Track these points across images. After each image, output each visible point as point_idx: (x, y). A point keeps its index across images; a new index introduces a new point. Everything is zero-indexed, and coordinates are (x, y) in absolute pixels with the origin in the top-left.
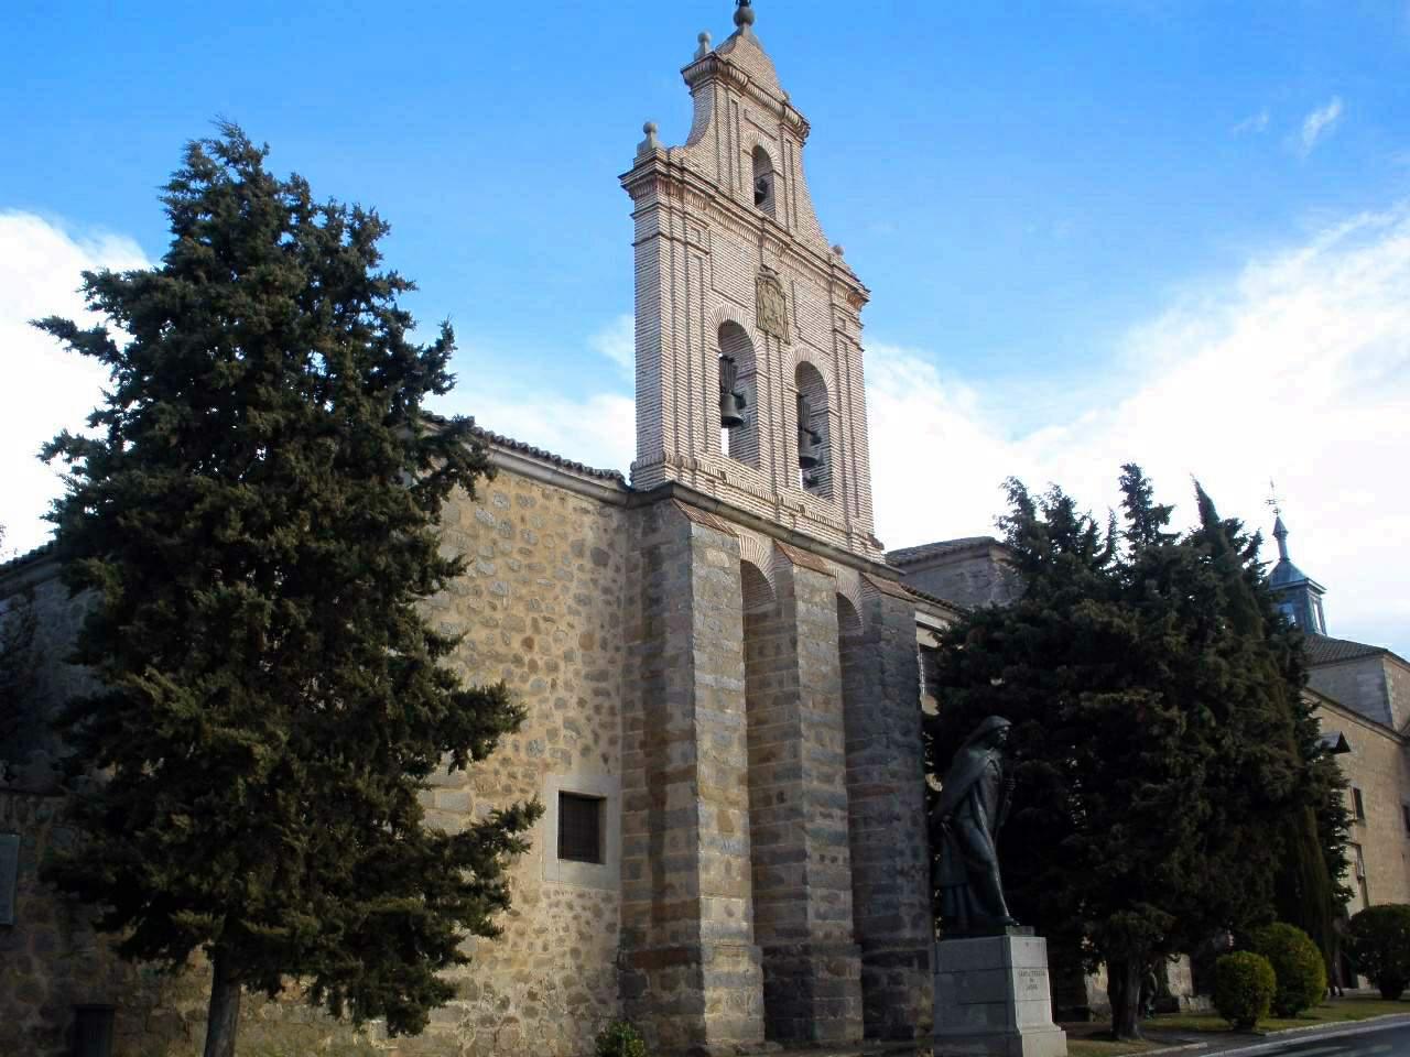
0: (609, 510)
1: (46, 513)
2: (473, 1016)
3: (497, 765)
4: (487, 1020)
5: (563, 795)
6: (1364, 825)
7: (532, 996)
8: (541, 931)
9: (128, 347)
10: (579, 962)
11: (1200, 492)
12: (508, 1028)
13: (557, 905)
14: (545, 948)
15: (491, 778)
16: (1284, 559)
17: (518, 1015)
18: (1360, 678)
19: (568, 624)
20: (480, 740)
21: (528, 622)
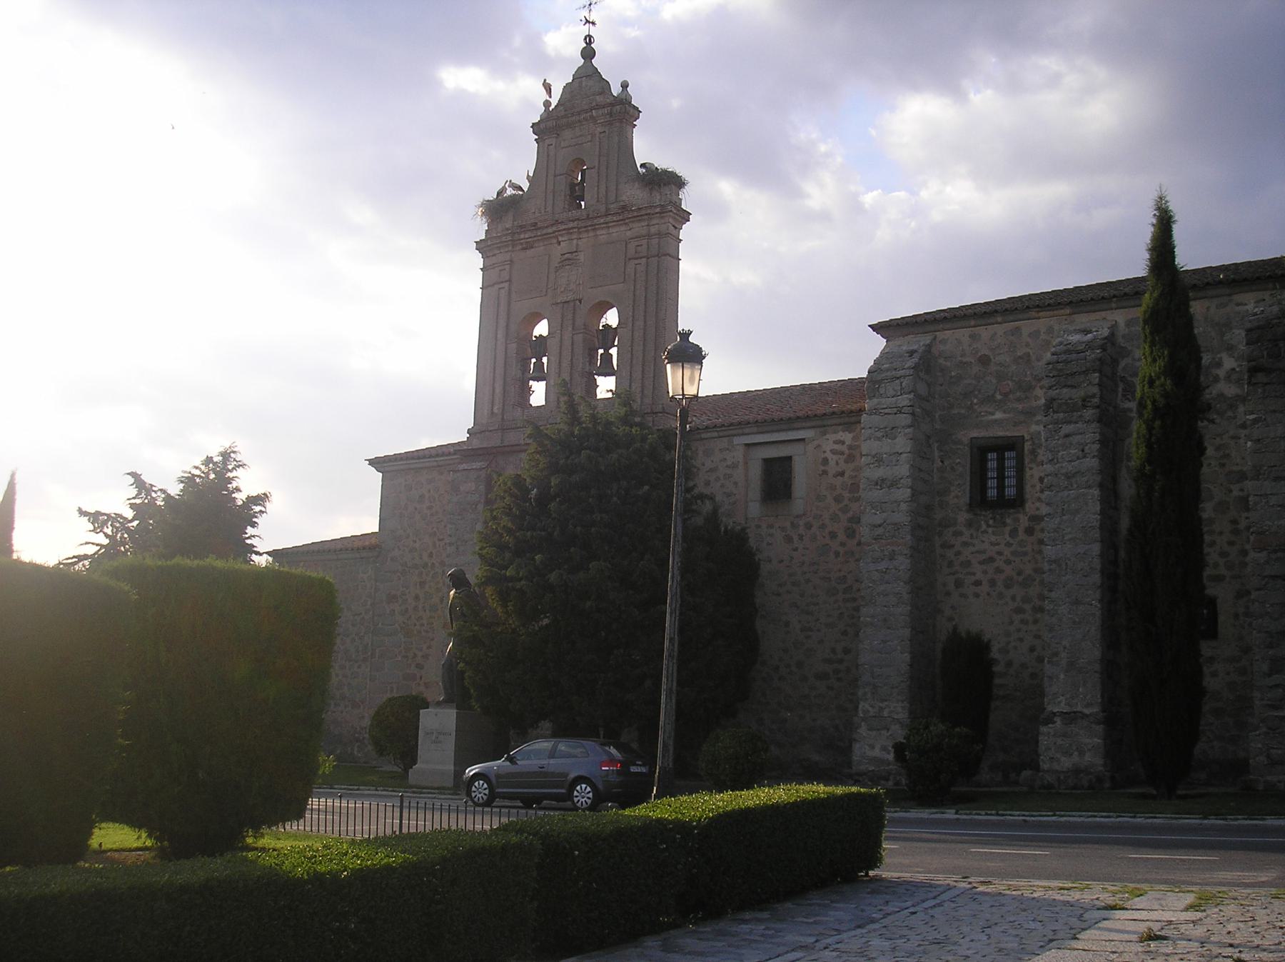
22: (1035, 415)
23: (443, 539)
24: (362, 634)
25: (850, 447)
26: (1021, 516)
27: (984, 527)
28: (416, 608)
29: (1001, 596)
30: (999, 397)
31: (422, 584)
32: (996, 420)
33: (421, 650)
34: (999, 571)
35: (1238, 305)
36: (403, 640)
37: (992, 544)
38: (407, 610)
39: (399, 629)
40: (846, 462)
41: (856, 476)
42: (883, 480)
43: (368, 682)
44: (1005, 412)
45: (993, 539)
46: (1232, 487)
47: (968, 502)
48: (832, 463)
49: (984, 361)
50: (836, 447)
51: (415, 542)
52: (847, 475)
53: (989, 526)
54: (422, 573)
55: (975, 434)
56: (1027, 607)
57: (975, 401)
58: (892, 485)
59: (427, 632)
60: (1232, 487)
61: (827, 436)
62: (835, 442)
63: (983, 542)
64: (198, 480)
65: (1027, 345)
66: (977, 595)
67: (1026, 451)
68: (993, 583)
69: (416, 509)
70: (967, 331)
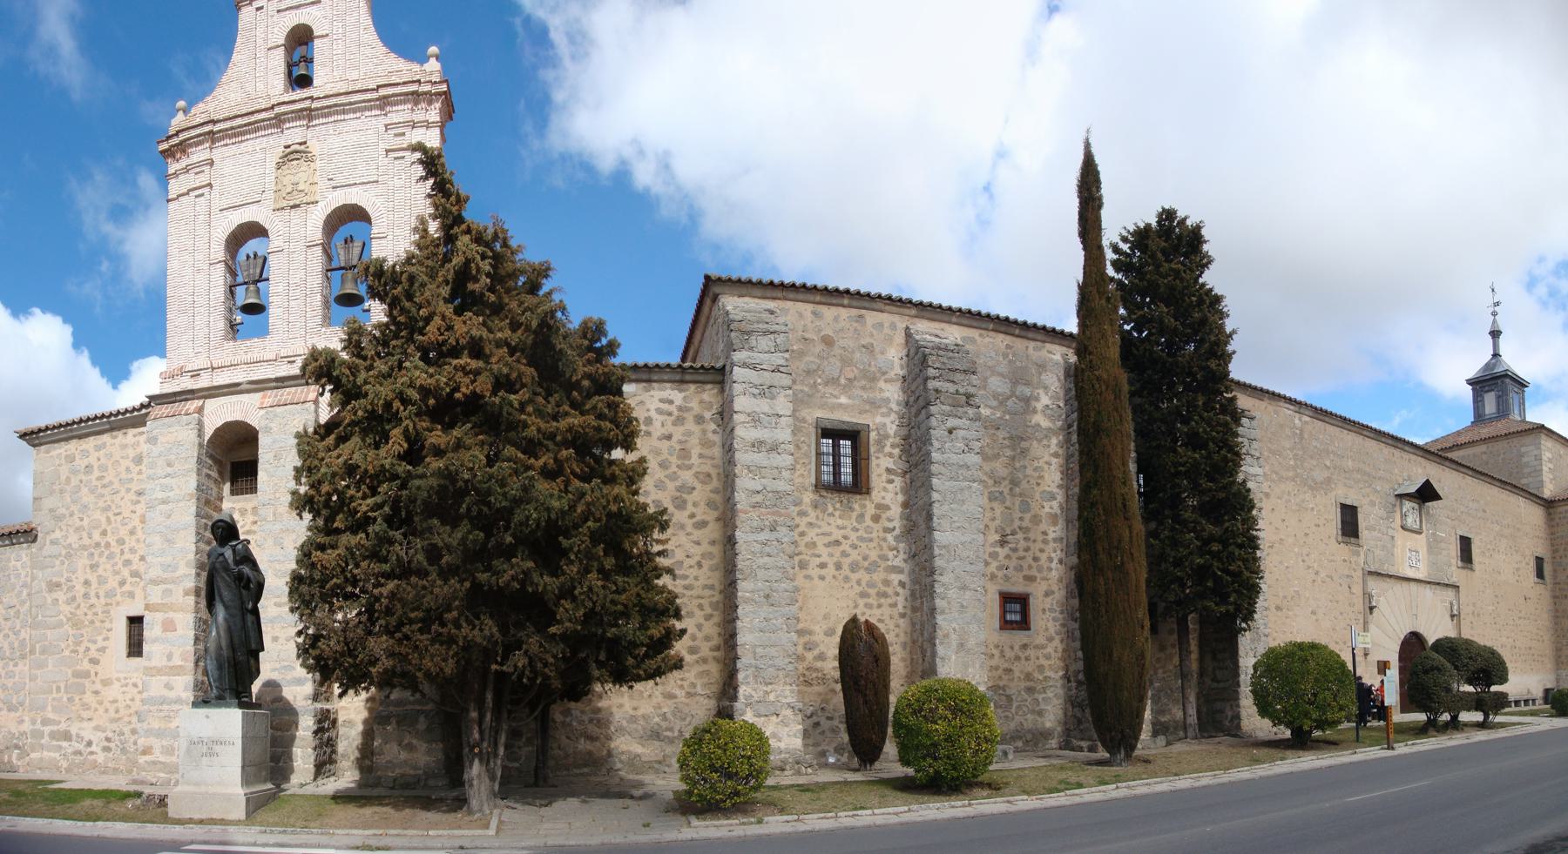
2: (70, 750)
3: (86, 610)
4: (79, 753)
6: (1472, 569)
7: (108, 740)
8: (115, 701)
9: (22, 318)
11: (1087, 146)
12: (91, 757)
13: (126, 685)
14: (117, 711)
15: (82, 617)
16: (1496, 355)
18: (1523, 449)
20: (555, 141)
21: (103, 520)
22: (880, 407)
23: (119, 514)
24: (18, 628)
25: (680, 409)
26: (867, 502)
27: (831, 509)
28: (86, 595)
29: (847, 579)
30: (843, 381)
31: (94, 567)
32: (841, 404)
33: (95, 642)
34: (844, 554)
35: (1050, 352)
36: (71, 632)
37: (838, 527)
38: (74, 598)
39: (65, 620)
40: (674, 424)
41: (686, 441)
42: (761, 442)
43: (27, 681)
44: (850, 398)
45: (840, 522)
46: (1045, 504)
47: (814, 482)
48: (657, 424)
49: (828, 341)
50: (665, 407)
51: (82, 520)
52: (675, 439)
53: (835, 509)
54: (93, 554)
55: (819, 414)
56: (872, 592)
57: (819, 381)
58: (772, 449)
59: (103, 622)
60: (1045, 504)
61: (652, 393)
62: (661, 401)
63: (829, 524)
64: (699, 805)
65: (872, 335)
66: (822, 578)
67: (872, 442)
68: (838, 567)
69: (81, 481)
70: (810, 307)
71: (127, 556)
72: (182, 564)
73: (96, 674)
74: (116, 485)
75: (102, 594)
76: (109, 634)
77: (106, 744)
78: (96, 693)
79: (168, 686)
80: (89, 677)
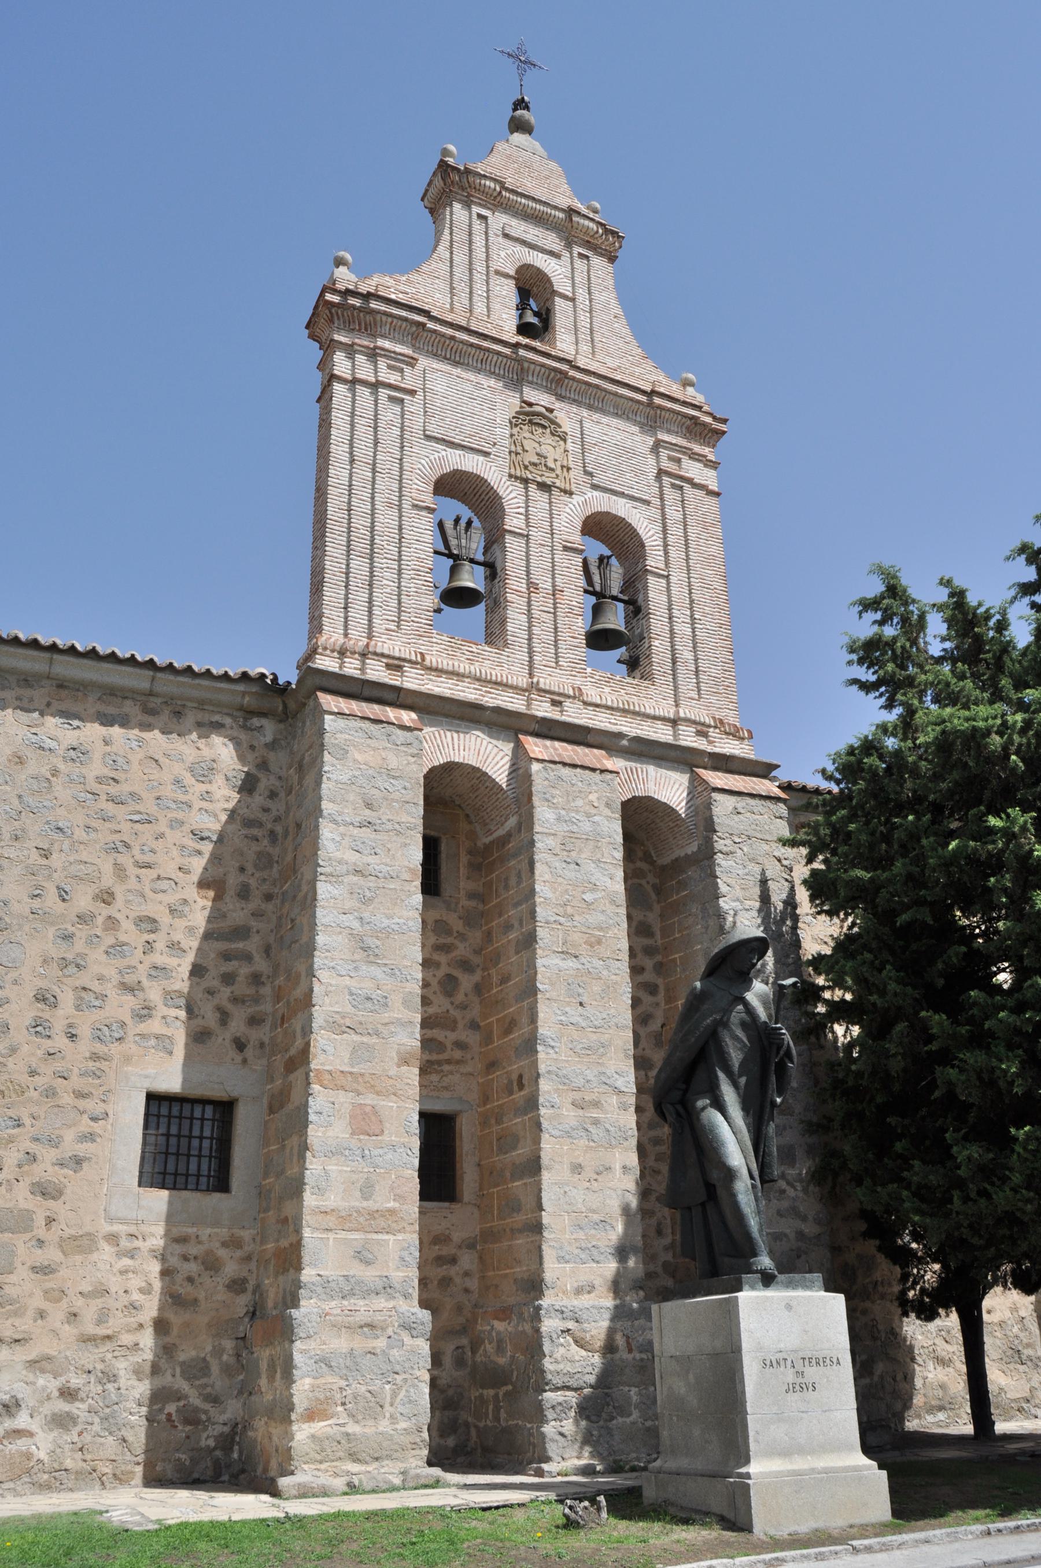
0: (256, 722)
1: (535, 70)
5: (152, 1097)
7: (68, 1394)
10: (167, 1340)
17: (34, 1426)
19: (34, 1269)
33: (54, 1142)
59: (80, 1095)
71: (160, 958)
72: (396, 1000)
73: (50, 1221)
74: (149, 806)
75: (84, 1031)
76: (97, 1127)
77: (62, 1406)
78: (44, 1270)
79: (363, 1256)
80: (28, 1229)
